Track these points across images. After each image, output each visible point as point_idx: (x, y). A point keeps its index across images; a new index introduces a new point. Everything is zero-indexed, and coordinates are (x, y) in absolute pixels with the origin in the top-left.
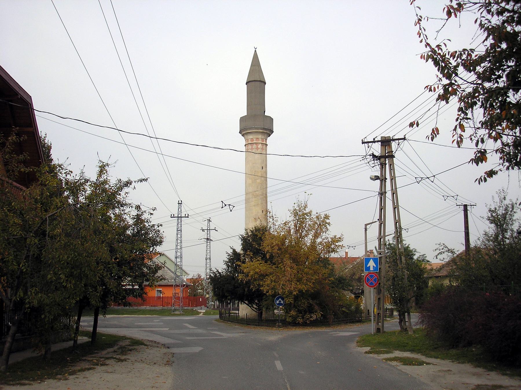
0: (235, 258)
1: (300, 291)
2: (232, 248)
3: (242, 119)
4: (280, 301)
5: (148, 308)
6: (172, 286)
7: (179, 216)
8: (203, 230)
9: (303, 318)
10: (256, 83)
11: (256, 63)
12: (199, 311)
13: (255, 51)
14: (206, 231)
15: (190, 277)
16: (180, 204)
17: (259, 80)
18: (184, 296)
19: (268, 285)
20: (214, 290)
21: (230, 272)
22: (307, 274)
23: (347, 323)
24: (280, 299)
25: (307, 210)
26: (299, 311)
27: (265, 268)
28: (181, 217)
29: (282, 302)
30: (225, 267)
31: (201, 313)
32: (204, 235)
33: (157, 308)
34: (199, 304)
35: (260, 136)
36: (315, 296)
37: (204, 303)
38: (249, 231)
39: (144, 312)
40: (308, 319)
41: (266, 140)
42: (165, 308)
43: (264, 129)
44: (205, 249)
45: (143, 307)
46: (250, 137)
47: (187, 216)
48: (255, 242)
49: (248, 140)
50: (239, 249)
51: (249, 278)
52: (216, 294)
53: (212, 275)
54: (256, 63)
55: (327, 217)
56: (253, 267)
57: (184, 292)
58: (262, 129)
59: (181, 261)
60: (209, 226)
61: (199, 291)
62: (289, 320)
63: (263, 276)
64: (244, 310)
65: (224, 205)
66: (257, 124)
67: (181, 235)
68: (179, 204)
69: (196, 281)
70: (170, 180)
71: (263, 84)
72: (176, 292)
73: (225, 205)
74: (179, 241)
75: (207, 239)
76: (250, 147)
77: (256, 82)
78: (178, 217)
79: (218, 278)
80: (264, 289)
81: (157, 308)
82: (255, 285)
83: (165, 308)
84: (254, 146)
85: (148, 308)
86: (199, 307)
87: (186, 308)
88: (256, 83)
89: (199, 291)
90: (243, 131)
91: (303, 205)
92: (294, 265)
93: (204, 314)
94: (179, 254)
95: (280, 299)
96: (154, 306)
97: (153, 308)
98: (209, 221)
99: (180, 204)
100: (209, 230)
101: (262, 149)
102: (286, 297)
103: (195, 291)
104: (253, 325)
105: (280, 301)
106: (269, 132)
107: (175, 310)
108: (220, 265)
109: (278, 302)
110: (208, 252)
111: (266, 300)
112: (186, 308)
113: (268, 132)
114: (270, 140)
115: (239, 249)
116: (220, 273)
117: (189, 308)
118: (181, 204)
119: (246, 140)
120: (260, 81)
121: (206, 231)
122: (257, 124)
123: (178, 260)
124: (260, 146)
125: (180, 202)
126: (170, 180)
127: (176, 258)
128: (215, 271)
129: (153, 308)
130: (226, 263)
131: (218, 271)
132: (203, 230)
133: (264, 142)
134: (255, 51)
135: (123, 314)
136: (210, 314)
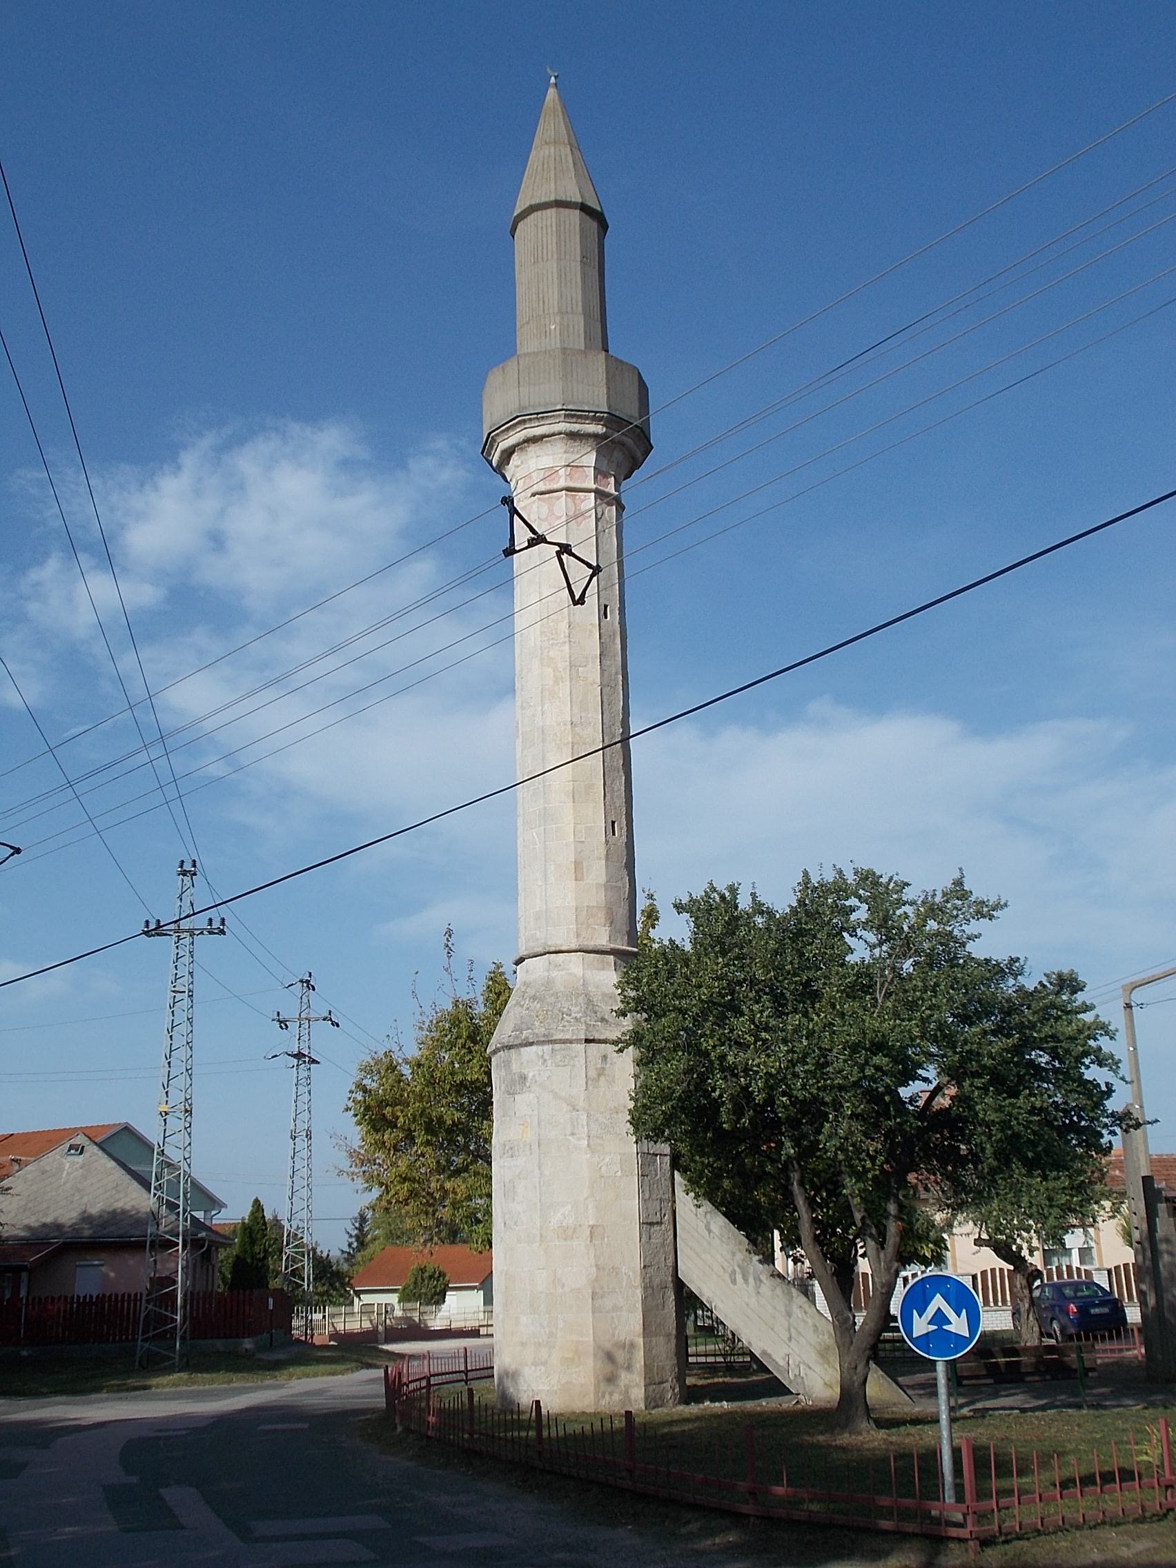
75: (299, 1056)
132: (283, 1024)
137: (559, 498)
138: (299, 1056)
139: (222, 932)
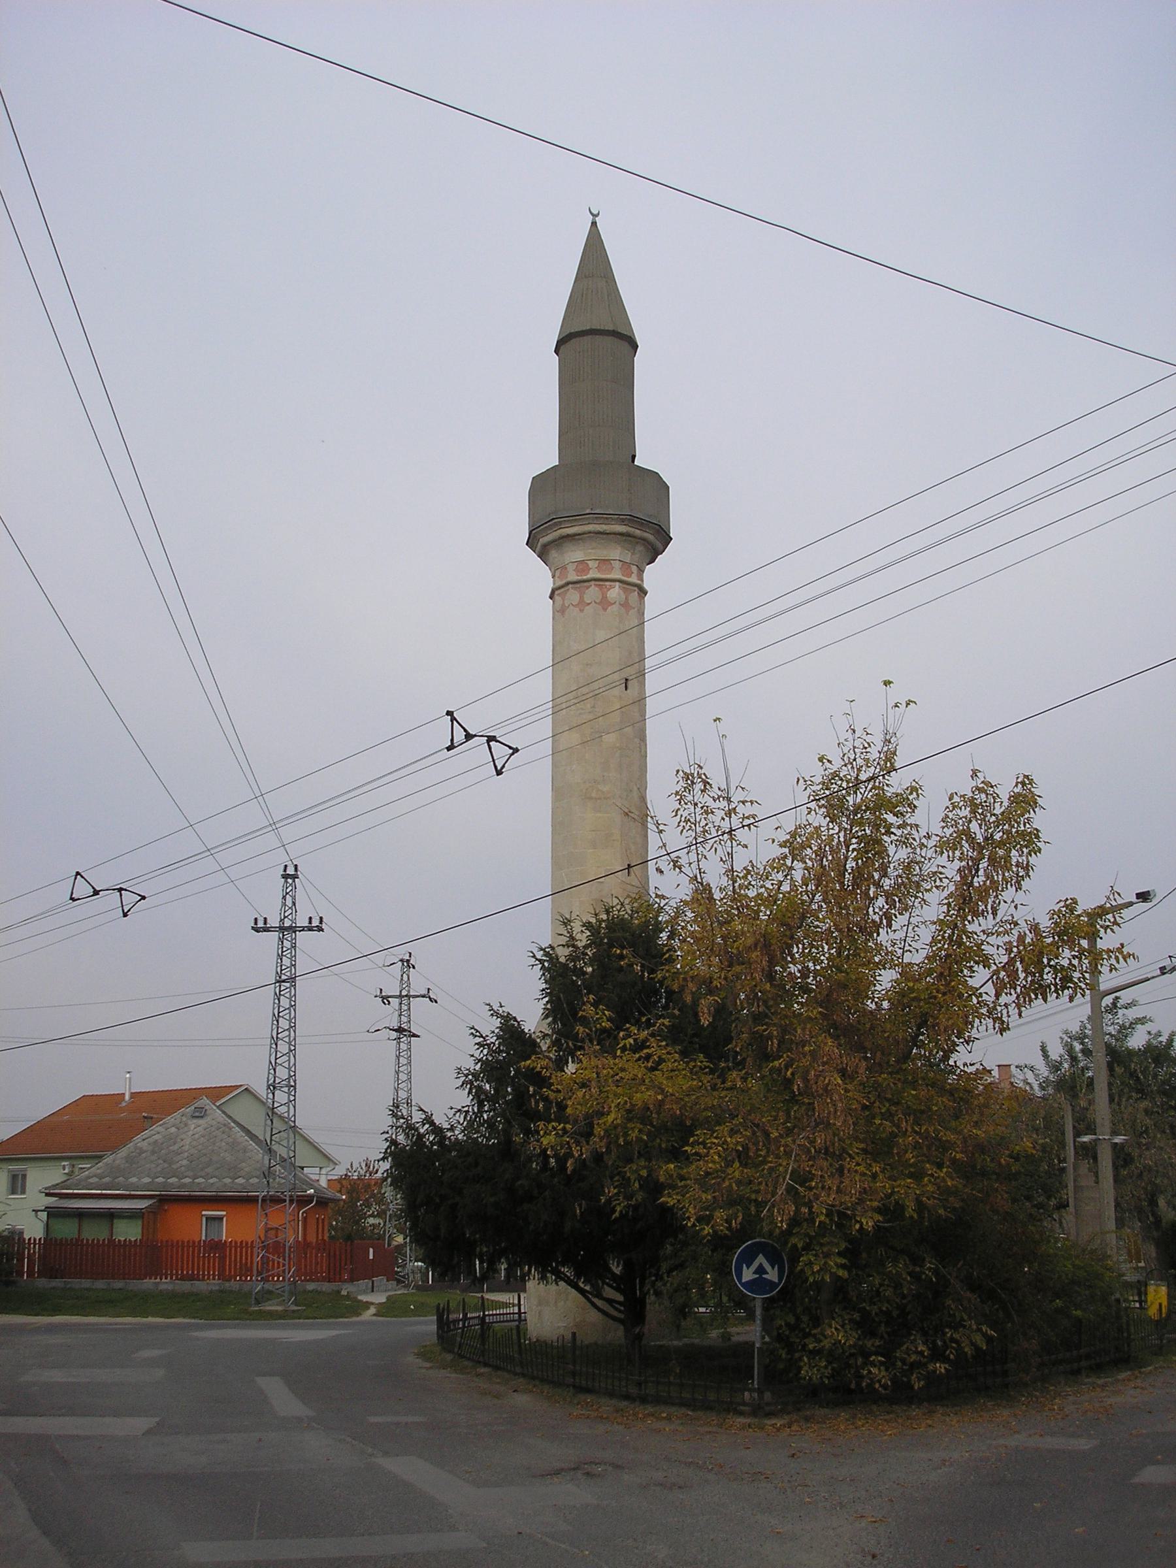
0: (508, 1067)
1: (891, 1211)
2: (495, 1014)
3: (541, 485)
4: (761, 1270)
5: (166, 1284)
6: (252, 1200)
7: (287, 923)
8: (385, 999)
9: (888, 1365)
10: (597, 345)
11: (595, 266)
12: (363, 1298)
13: (594, 224)
14: (395, 1002)
15: (340, 1171)
16: (290, 877)
17: (611, 328)
18: (312, 1238)
19: (703, 1182)
20: (411, 1209)
21: (491, 1124)
22: (919, 1115)
23: (1076, 1372)
24: (761, 1259)
25: (896, 783)
26: (866, 1326)
27: (685, 1083)
28: (293, 929)
29: (772, 1275)
30: (464, 1099)
31: (367, 1305)
32: (389, 1015)
33: (201, 1286)
34: (365, 1272)
35: (616, 553)
36: (946, 1236)
37: (386, 1266)
38: (577, 927)
39: (141, 1304)
40: (913, 1366)
41: (641, 571)
42: (233, 1285)
43: (633, 520)
44: (392, 1068)
45: (148, 1284)
46: (574, 554)
47: (315, 923)
48: (614, 973)
49: (564, 568)
50: (532, 1016)
51: (598, 1143)
52: (421, 1237)
53: (401, 1138)
54: (595, 266)
55: (1025, 800)
56: (611, 1085)
57: (312, 1223)
58: (622, 522)
59: (292, 1102)
60: (405, 982)
61: (371, 1221)
62: (812, 1371)
63: (675, 1134)
64: (546, 1307)
65: (460, 735)
66: (600, 509)
67: (293, 998)
68: (286, 877)
69: (356, 1188)
70: (234, 743)
71: (626, 346)
72: (273, 1223)
73: (469, 737)
74: (284, 1024)
75: (400, 1030)
76: (573, 595)
77: (598, 339)
78: (282, 929)
79: (433, 1156)
80: (688, 1202)
81: (201, 1286)
82: (626, 1183)
83: (233, 1285)
84: (592, 592)
85: (166, 1284)
86: (364, 1284)
87: (311, 1286)
88: (597, 345)
89: (371, 1221)
90: (544, 538)
91: (874, 754)
92: (853, 1061)
93: (385, 1310)
94: (282, 1073)
95: (761, 1259)
96: (192, 1278)
97: (186, 1286)
98: (407, 964)
99: (290, 877)
100: (405, 997)
101: (625, 605)
102: (807, 1248)
103: (357, 1223)
104: (611, 1394)
105: (761, 1270)
106: (652, 537)
107: (266, 1295)
108: (445, 1098)
109: (748, 1275)
110: (403, 1077)
111: (681, 1266)
112: (311, 1286)
113: (650, 537)
114: (654, 575)
115: (532, 1016)
116: (437, 1130)
117: (326, 1287)
118: (294, 877)
119: (557, 570)
120: (615, 334)
121: (395, 1002)
122: (600, 509)
123: (281, 1097)
124: (615, 592)
125: (291, 871)
126: (234, 743)
127: (273, 1087)
128: (417, 1117)
129: (186, 1286)
130: (470, 1081)
131: (429, 1120)
132: (385, 999)
133: (634, 579)
134: (594, 224)
135: (56, 1310)
136: (406, 1312)
137: (588, 588)
138: (400, 1030)
139: (320, 929)
